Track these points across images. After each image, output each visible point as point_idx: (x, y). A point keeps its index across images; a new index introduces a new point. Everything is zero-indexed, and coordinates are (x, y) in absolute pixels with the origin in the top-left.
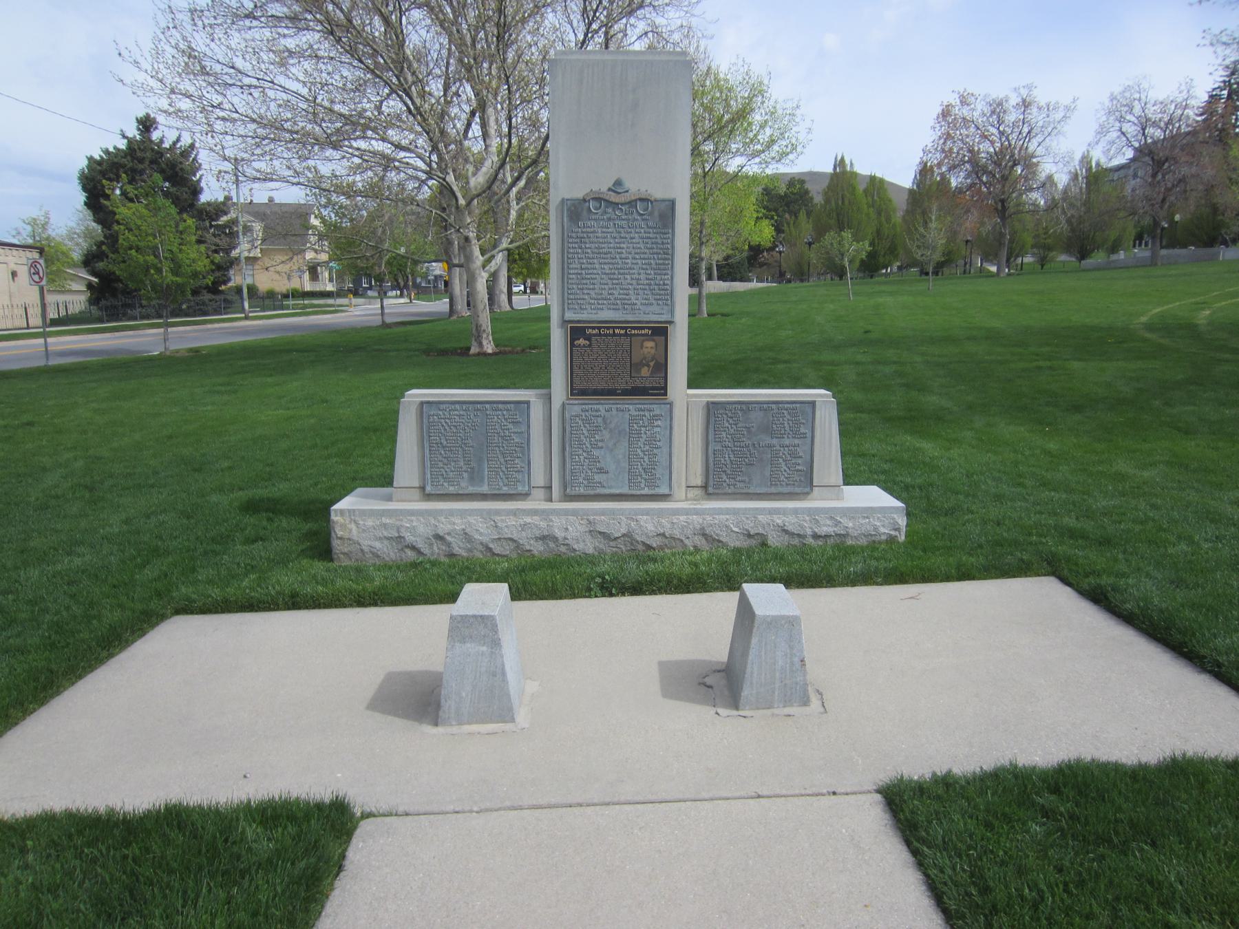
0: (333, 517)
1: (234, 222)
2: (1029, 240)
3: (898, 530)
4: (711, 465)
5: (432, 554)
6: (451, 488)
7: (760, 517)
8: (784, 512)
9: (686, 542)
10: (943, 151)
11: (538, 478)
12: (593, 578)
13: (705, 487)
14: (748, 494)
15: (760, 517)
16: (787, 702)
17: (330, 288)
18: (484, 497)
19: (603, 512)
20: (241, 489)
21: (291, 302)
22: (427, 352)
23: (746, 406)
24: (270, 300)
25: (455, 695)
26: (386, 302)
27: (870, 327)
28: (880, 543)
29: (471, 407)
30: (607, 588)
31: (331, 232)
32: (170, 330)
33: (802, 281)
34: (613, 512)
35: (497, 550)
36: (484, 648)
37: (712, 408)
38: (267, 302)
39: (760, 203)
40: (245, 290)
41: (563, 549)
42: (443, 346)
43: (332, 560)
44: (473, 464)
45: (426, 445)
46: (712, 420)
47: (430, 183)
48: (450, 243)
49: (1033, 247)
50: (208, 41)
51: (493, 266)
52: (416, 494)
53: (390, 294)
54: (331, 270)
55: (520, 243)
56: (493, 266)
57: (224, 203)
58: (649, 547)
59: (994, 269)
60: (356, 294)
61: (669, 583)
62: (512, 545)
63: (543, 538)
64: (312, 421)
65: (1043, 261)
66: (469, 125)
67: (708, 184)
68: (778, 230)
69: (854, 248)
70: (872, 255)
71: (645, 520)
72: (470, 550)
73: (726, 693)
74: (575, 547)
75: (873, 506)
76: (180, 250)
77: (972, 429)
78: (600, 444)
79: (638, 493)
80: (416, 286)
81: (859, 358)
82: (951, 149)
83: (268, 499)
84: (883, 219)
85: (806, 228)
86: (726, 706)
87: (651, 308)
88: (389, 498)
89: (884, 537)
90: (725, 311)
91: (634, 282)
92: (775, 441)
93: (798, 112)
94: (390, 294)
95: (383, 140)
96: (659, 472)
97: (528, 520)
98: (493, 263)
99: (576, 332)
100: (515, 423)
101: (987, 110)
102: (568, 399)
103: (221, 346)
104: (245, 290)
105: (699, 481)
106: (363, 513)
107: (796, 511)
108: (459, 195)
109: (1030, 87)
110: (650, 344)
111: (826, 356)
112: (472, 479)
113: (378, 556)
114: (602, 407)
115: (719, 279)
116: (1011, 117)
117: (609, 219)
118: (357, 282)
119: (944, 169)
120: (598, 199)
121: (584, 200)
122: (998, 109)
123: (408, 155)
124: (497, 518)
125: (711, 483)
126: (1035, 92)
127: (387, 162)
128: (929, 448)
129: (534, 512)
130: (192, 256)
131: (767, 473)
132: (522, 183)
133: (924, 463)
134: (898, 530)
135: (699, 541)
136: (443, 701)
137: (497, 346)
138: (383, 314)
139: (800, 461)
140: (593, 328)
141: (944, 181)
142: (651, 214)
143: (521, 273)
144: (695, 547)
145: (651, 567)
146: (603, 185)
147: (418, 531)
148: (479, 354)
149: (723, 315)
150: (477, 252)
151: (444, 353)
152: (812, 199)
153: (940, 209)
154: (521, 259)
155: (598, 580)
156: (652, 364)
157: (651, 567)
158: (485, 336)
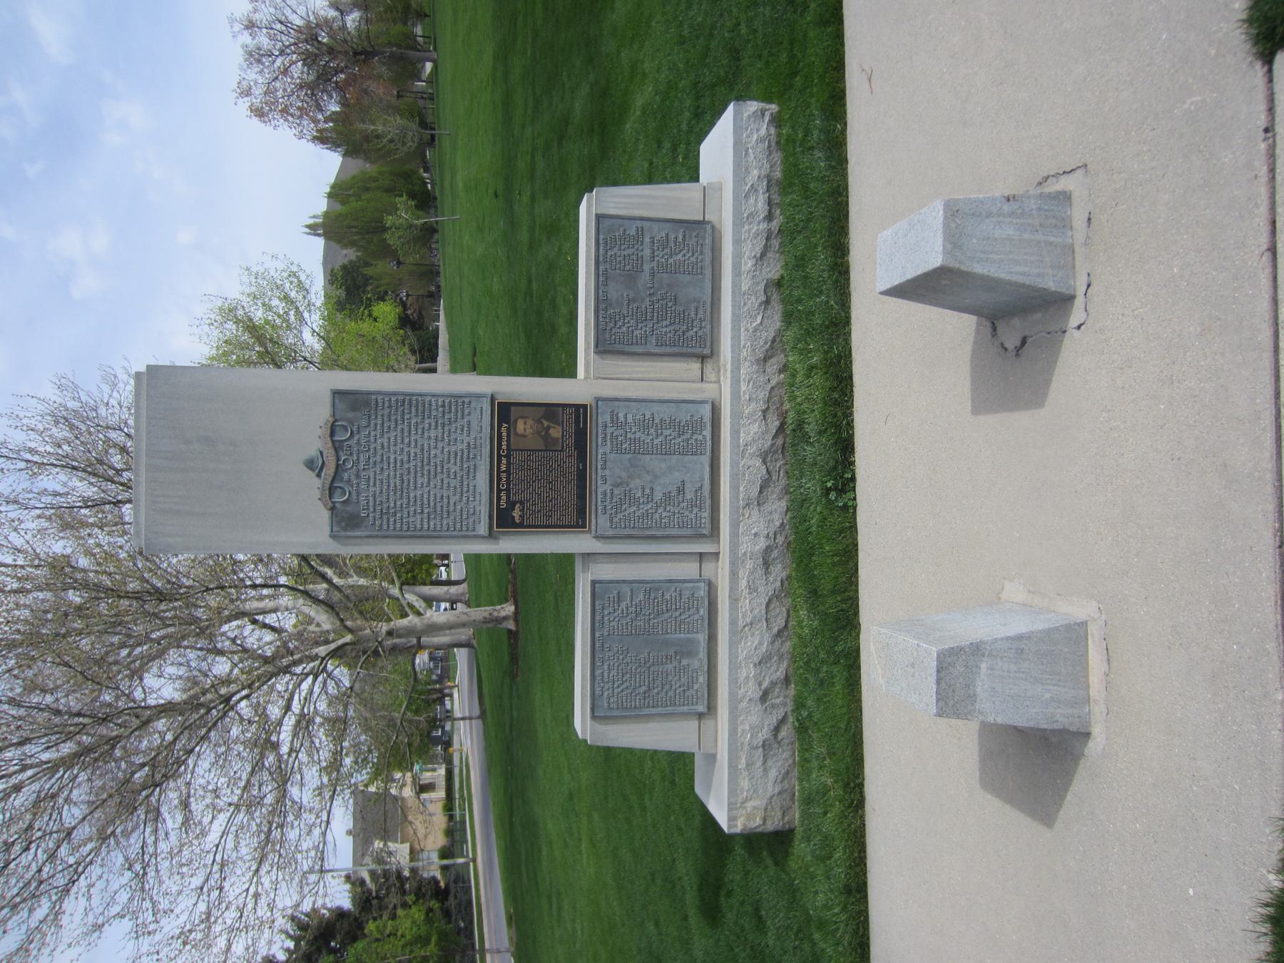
0: (738, 829)
1: (373, 873)
2: (399, 28)
3: (763, 112)
4: (676, 350)
5: (785, 704)
6: (701, 680)
7: (744, 288)
8: (737, 257)
9: (773, 383)
10: (300, 117)
11: (688, 570)
12: (829, 502)
13: (703, 358)
14: (712, 304)
15: (744, 288)
16: (1065, 224)
17: (442, 771)
18: (712, 638)
19: (735, 488)
20: (686, 918)
21: (457, 812)
22: (514, 676)
23: (601, 304)
24: (455, 832)
25: (1036, 707)
26: (458, 714)
27: (491, 191)
28: (779, 135)
29: (598, 655)
30: (844, 485)
31: (382, 771)
32: (487, 946)
33: (438, 273)
34: (735, 477)
35: (780, 622)
36: (984, 666)
37: (604, 347)
38: (457, 836)
39: (352, 316)
40: (446, 862)
41: (780, 540)
42: (507, 659)
43: (792, 831)
44: (671, 652)
45: (646, 711)
46: (618, 347)
47: (330, 667)
48: (394, 649)
49: (405, 23)
50: (173, 916)
51: (420, 604)
52: (708, 724)
53: (448, 707)
54: (422, 770)
55: (394, 574)
56: (420, 604)
57: (353, 884)
58: (781, 429)
59: (429, 66)
60: (448, 744)
61: (836, 403)
62: (775, 604)
63: (766, 564)
64: (596, 816)
65: (422, 15)
66: (265, 626)
67: (332, 360)
68: (382, 298)
69: (403, 214)
70: (412, 196)
71: (744, 434)
72: (781, 658)
73: (1038, 316)
74: (778, 524)
75: (731, 149)
76: (402, 936)
77: (619, 52)
78: (647, 491)
79: (709, 443)
80: (441, 680)
81: (526, 198)
82: (299, 108)
83: (700, 890)
84: (374, 185)
85: (382, 268)
86: (1066, 314)
87: (474, 425)
88: (712, 758)
89: (773, 131)
90: (469, 352)
91: (440, 445)
92: (647, 267)
93: (254, 269)
94: (448, 707)
95: (280, 723)
96: (683, 417)
97: (743, 583)
98: (416, 604)
99: (504, 521)
100: (619, 598)
101: (257, 68)
102: (590, 531)
103: (505, 891)
104: (446, 862)
105: (695, 366)
106: (733, 792)
107: (737, 242)
108: (340, 642)
109: (232, 21)
110: (521, 426)
111: (524, 236)
112: (690, 654)
113: (787, 773)
114: (601, 487)
115: (435, 360)
116: (264, 42)
117: (358, 476)
118: (436, 741)
119: (320, 117)
120: (332, 490)
121: (333, 509)
122: (255, 56)
123: (296, 697)
124: (741, 623)
125: (698, 350)
126: (238, 15)
127: (304, 723)
128: (643, 97)
129: (734, 575)
130: (408, 924)
131: (688, 278)
132: (329, 572)
133: (663, 101)
134: (763, 112)
135: (773, 366)
136: (1055, 726)
137: (507, 601)
138: (470, 718)
139: (672, 237)
140: (499, 498)
141: (332, 118)
142: (351, 422)
143: (427, 571)
144: (780, 371)
145: (811, 428)
146: (313, 485)
147: (757, 723)
148: (516, 621)
149: (474, 355)
150: (404, 622)
151: (514, 658)
152: (351, 262)
153: (363, 122)
154: (412, 570)
155: (832, 496)
156: (546, 424)
157: (811, 428)
158: (495, 614)
